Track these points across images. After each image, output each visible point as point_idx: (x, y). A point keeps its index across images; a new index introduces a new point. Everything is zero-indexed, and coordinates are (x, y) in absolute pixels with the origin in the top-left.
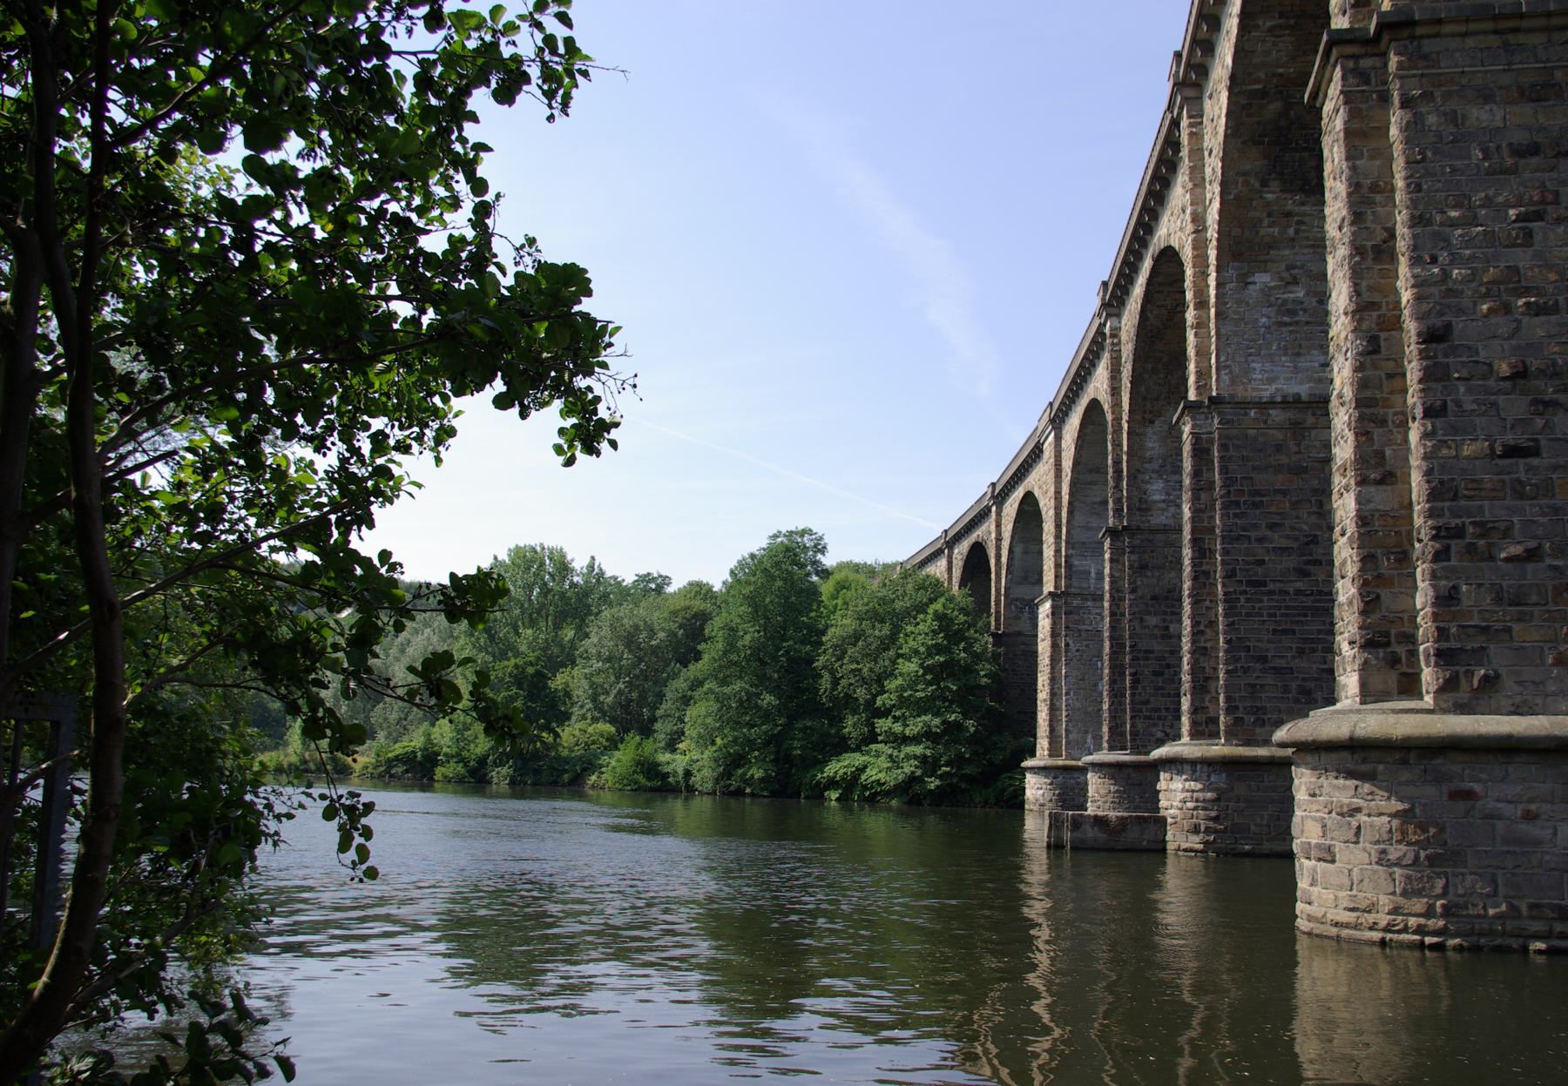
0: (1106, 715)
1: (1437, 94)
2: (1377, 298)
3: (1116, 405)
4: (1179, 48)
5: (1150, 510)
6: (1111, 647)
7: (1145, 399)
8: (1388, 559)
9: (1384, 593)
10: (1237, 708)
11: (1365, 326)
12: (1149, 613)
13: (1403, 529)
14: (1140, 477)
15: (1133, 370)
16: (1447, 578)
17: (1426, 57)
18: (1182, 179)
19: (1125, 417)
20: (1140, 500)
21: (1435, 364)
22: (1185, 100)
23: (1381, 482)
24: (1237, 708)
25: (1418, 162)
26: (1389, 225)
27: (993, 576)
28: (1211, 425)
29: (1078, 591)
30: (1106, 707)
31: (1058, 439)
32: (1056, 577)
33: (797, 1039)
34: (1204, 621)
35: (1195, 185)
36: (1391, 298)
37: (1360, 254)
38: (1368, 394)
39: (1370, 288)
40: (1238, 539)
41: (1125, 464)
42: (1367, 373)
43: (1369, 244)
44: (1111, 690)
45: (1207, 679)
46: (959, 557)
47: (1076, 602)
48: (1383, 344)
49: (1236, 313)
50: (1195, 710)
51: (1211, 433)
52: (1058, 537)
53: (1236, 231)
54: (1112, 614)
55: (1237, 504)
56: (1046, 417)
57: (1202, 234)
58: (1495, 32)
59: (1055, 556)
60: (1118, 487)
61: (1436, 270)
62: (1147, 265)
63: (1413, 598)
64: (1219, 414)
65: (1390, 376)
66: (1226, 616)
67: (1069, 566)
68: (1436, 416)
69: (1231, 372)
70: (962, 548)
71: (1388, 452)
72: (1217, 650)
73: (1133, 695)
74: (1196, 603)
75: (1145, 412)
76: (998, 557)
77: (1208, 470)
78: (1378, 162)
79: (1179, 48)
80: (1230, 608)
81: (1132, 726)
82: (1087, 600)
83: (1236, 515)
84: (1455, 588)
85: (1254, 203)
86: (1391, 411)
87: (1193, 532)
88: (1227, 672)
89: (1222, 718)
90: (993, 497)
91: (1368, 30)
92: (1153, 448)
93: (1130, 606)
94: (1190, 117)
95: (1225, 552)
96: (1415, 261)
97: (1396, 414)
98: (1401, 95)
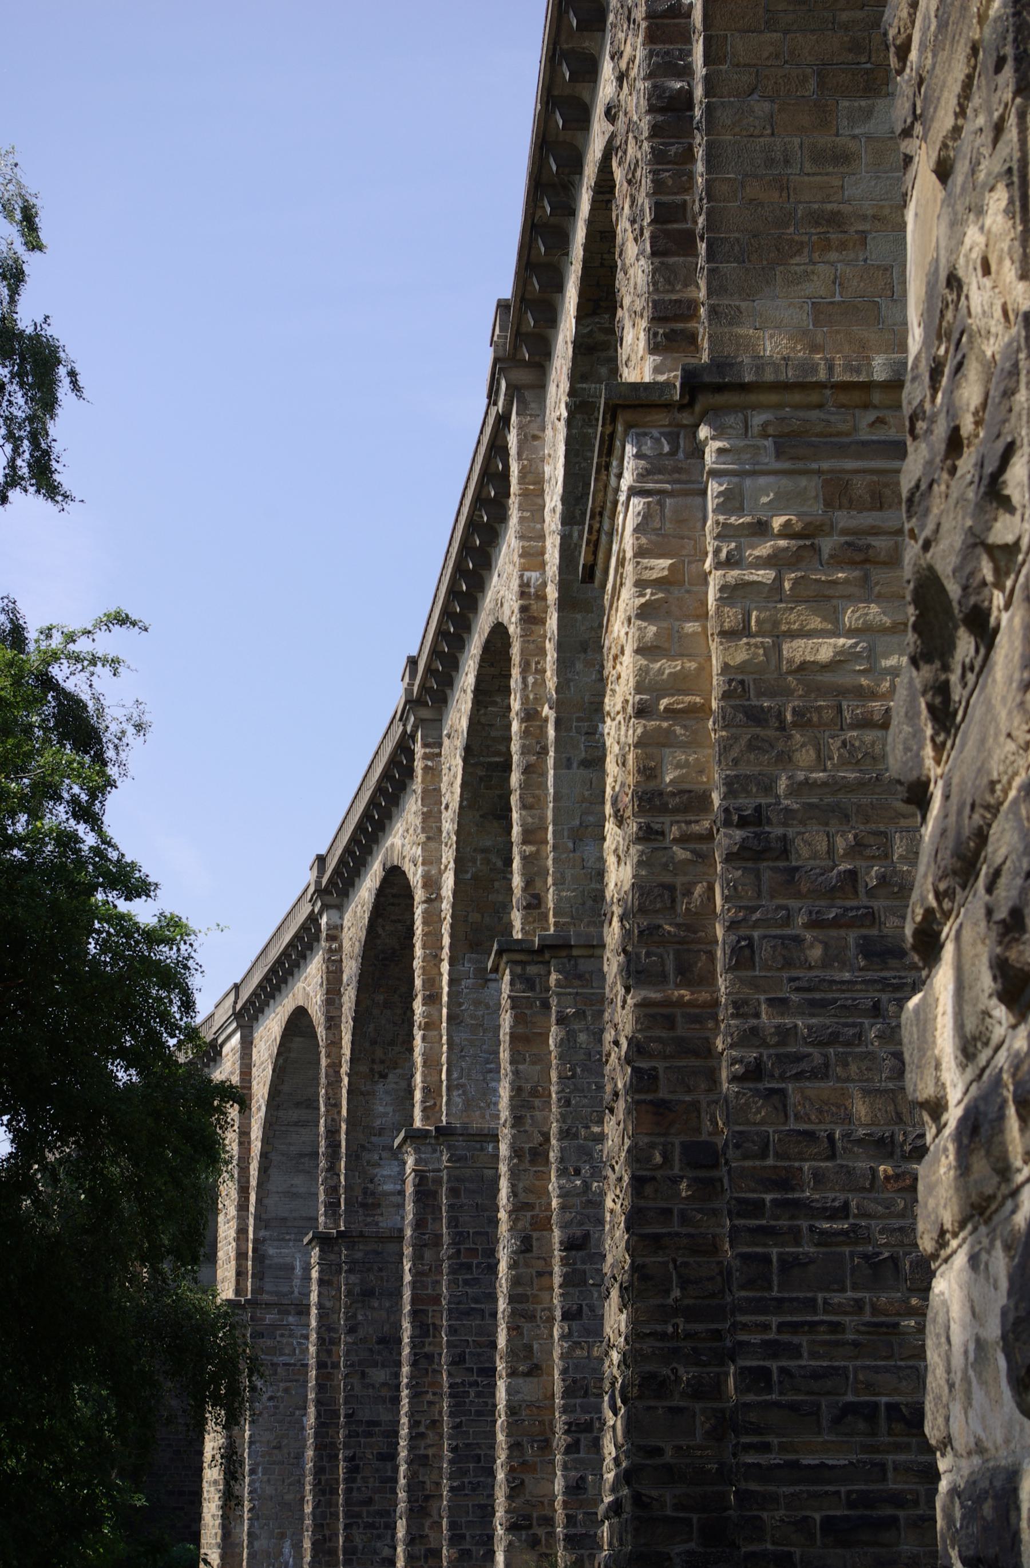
0: (308, 1522)
1: (588, 1013)
2: (531, 1199)
3: (333, 1022)
4: (414, 653)
5: (379, 1205)
6: (318, 1416)
7: (374, 1042)
8: (532, 1447)
9: (528, 1479)
10: (463, 1537)
11: (520, 1225)
12: (375, 1365)
13: (546, 1418)
14: (366, 1156)
15: (358, 1003)
16: (576, 1469)
17: (580, 977)
18: (412, 807)
19: (345, 1068)
20: (365, 1192)
21: (574, 1271)
22: (420, 722)
23: (528, 1374)
24: (463, 1537)
25: (568, 1078)
26: (545, 1130)
28: (439, 1160)
29: (274, 1299)
30: (308, 1509)
31: (247, 1044)
32: (239, 1274)
34: (425, 1421)
35: (428, 838)
36: (543, 1201)
37: (518, 1156)
38: (520, 1290)
39: (526, 1190)
40: (468, 1313)
41: (343, 1136)
42: (521, 1270)
43: (527, 1146)
44: (317, 1483)
45: (427, 1498)
47: (270, 1318)
48: (534, 1243)
49: (472, 1017)
50: (412, 1540)
51: (439, 1170)
52: (242, 1207)
53: (475, 917)
54: (321, 1365)
55: (468, 1267)
57: (435, 904)
59: (237, 1239)
60: (332, 1169)
61: (578, 1182)
63: (553, 1483)
64: (449, 1148)
65: (540, 1274)
66: (451, 1415)
67: (259, 1257)
68: (573, 1320)
69: (465, 1093)
71: (535, 1346)
72: (441, 1458)
73: (348, 1491)
74: (414, 1397)
75: (373, 1061)
77: (434, 1219)
78: (538, 1067)
79: (415, 653)
80: (456, 1405)
81: (347, 1539)
82: (288, 1313)
83: (466, 1282)
84: (583, 1479)
85: (497, 884)
86: (539, 1307)
87: (414, 1301)
88: (452, 1489)
89: (444, 1551)
91: (533, 941)
92: (386, 1114)
93: (347, 1353)
94: (425, 745)
95: (452, 1331)
96: (562, 1173)
97: (543, 1310)
98: (558, 1012)
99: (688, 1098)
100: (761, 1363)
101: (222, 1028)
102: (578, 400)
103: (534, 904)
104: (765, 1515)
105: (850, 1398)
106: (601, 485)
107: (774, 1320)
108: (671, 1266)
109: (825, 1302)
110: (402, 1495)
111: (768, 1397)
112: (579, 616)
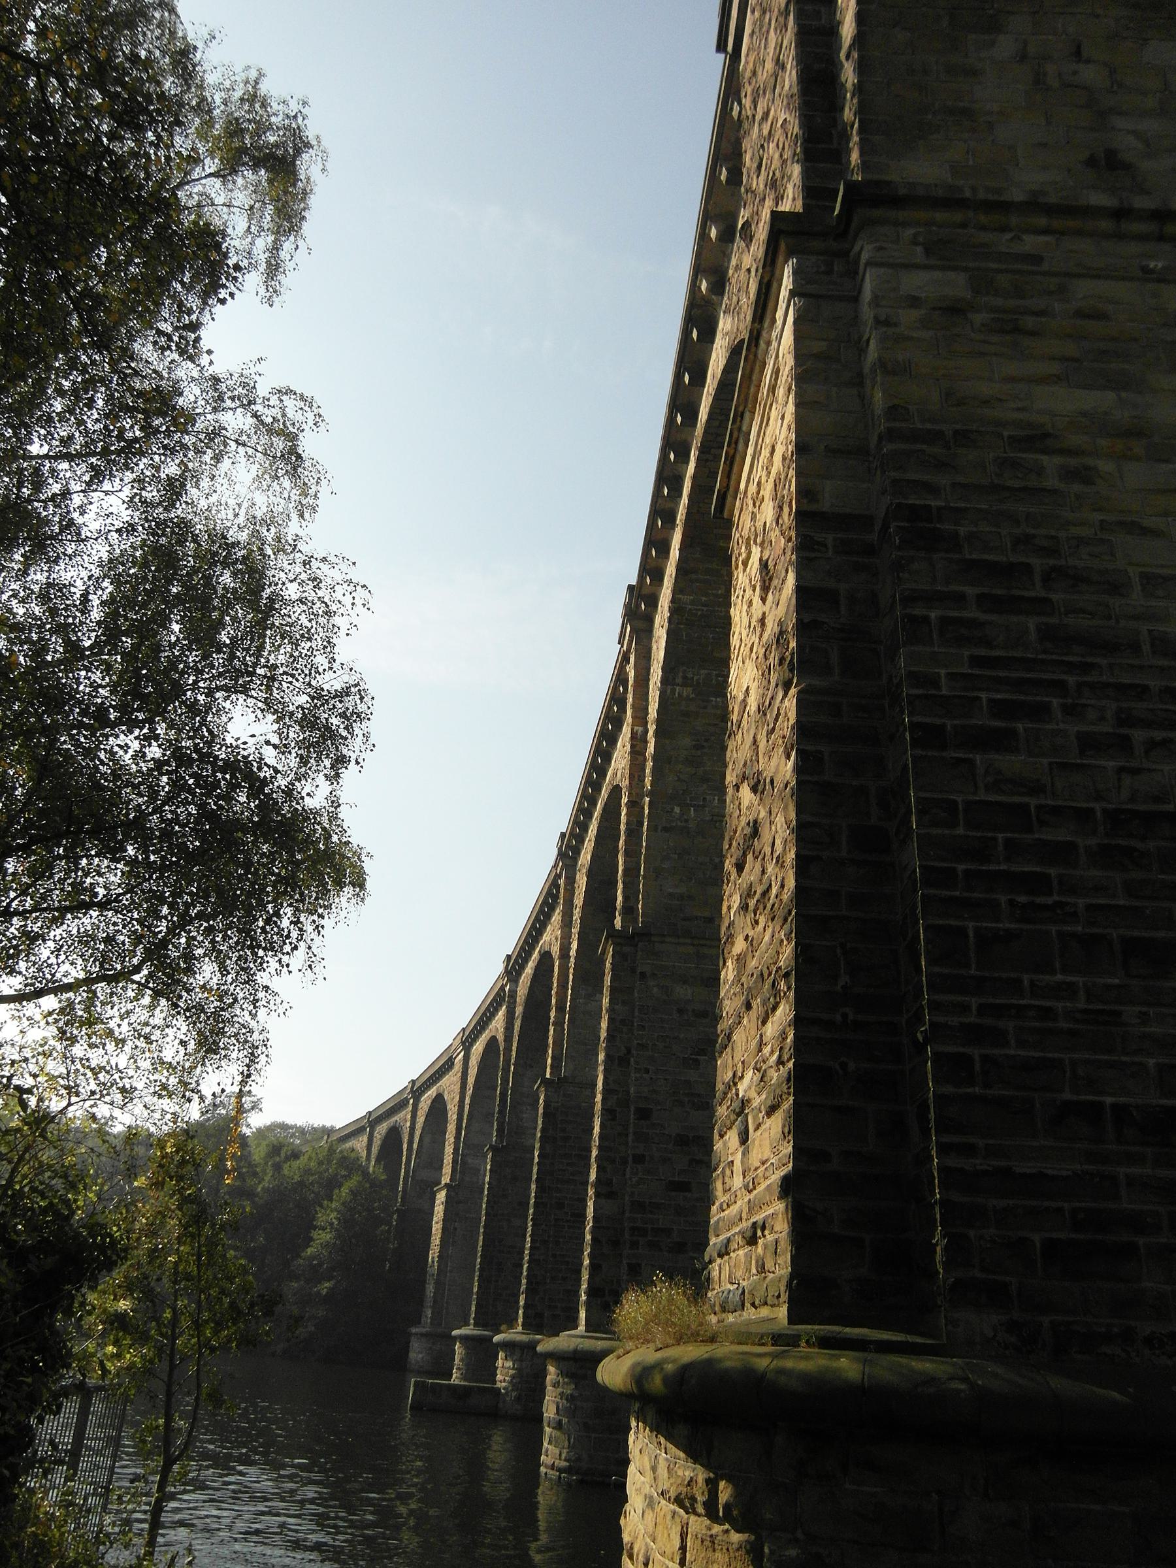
18: (556, 917)
27: (404, 1158)
33: (1145, 531)
46: (379, 1137)
56: (459, 1040)
58: (694, 945)
62: (535, 955)
67: (464, 1162)
70: (382, 1129)
76: (410, 1143)
90: (412, 1091)
99: (854, 783)
100: (961, 1050)
101: (456, 1050)
102: (676, 605)
103: (629, 910)
104: (972, 1233)
105: (1067, 1096)
106: (742, 397)
107: (974, 1002)
108: (839, 951)
109: (1032, 983)
110: (524, 1281)
111: (969, 1090)
112: (667, 742)
